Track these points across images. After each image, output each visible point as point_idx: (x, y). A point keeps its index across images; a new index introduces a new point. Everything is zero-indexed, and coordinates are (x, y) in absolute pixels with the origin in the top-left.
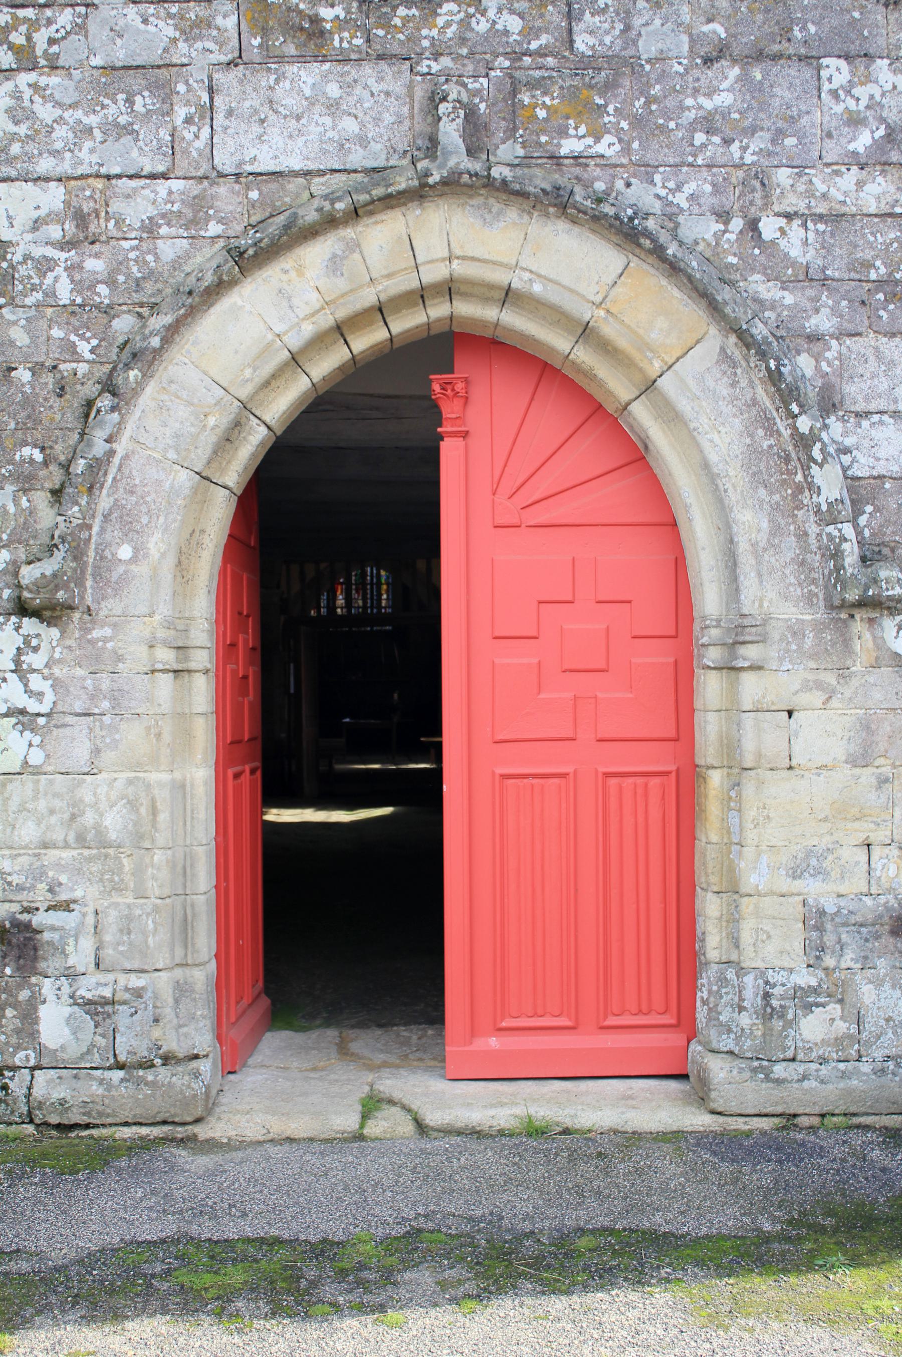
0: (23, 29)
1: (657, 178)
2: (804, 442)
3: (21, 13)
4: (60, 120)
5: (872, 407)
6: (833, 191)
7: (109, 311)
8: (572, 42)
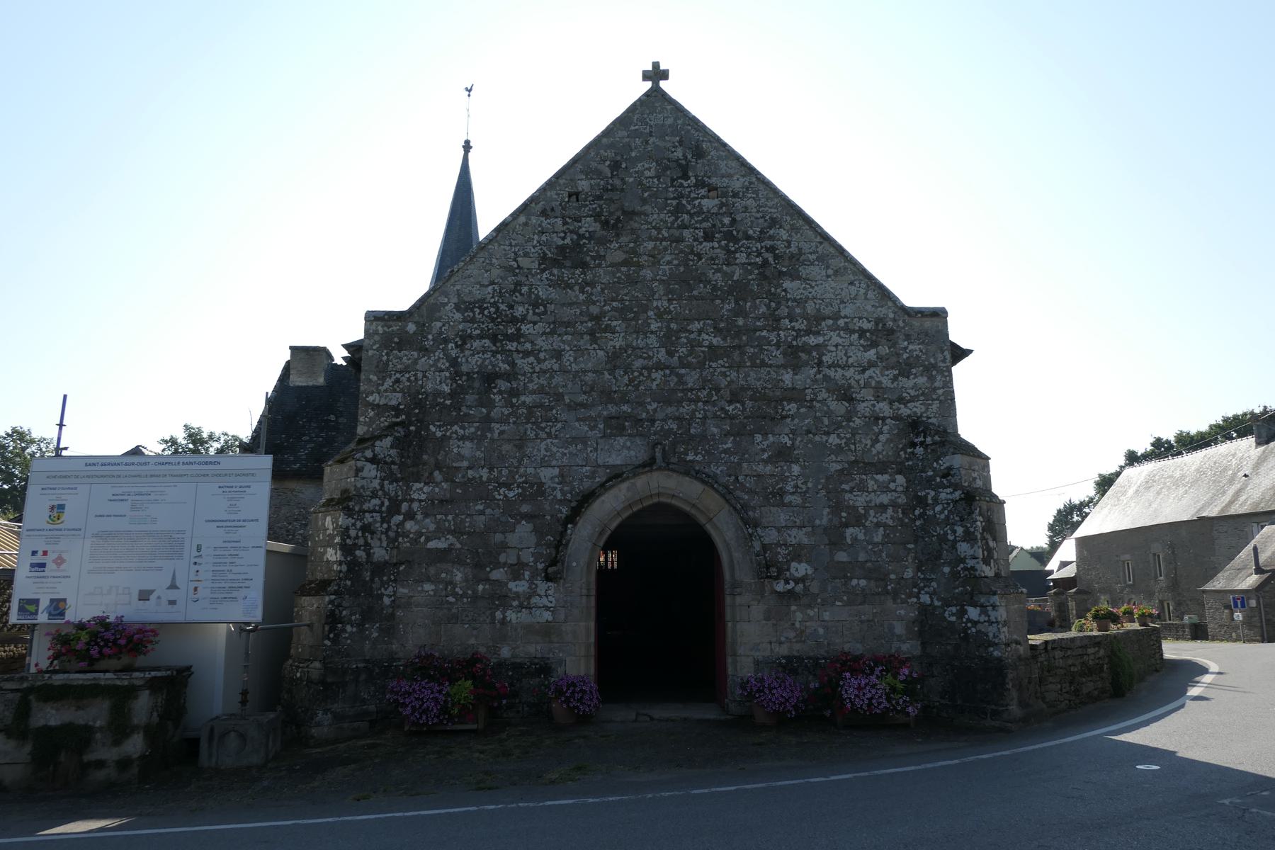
0: (549, 428)
1: (712, 466)
2: (751, 535)
3: (548, 424)
4: (558, 451)
5: (770, 525)
6: (758, 469)
7: (570, 501)
8: (689, 431)
